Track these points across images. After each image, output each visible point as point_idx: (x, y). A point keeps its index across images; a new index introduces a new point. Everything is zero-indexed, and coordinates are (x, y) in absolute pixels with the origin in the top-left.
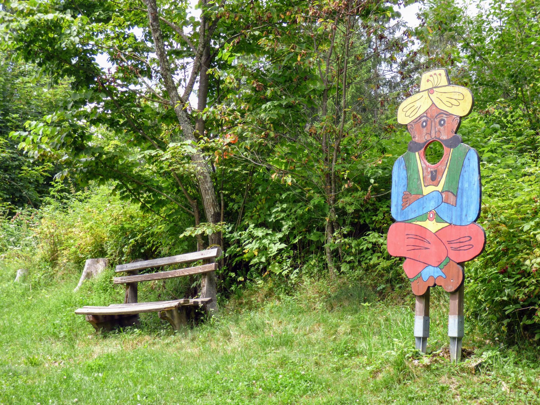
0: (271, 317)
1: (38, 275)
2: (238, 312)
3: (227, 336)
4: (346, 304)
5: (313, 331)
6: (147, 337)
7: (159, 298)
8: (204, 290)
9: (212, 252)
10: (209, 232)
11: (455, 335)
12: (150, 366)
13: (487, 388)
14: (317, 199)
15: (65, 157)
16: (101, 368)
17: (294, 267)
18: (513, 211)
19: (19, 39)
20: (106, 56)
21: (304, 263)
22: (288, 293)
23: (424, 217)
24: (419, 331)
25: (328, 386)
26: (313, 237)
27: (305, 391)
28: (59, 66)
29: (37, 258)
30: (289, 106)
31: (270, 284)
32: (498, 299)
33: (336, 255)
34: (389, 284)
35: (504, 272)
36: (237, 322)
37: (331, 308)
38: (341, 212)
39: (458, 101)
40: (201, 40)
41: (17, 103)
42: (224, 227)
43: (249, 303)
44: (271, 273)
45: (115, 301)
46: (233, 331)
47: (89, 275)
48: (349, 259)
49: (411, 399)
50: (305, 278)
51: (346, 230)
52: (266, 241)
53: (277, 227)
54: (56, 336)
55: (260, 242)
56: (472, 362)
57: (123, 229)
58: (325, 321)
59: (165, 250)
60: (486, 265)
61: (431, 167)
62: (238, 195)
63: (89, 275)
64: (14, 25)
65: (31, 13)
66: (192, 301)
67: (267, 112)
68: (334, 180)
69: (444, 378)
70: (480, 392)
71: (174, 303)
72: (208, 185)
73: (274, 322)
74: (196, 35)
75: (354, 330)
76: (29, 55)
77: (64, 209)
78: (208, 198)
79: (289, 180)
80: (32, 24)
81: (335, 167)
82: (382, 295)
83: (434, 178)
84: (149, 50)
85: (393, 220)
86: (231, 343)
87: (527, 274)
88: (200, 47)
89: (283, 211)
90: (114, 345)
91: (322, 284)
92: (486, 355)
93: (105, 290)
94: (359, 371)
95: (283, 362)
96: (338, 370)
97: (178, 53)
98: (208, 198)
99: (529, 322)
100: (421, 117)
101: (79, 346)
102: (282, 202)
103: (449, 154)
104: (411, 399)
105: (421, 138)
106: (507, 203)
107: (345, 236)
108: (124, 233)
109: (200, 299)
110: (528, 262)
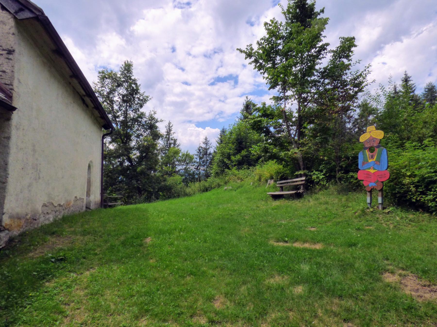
0: (322, 196)
1: (256, 184)
2: (311, 195)
3: (309, 201)
4: (344, 193)
5: (334, 200)
6: (287, 201)
7: (289, 191)
8: (302, 188)
9: (304, 178)
10: (302, 173)
11: (381, 202)
12: (289, 209)
13: (392, 219)
14: (334, 163)
15: (263, 154)
16: (275, 209)
17: (327, 182)
18: (398, 166)
19: (251, 125)
20: (272, 128)
21: (330, 181)
22: (326, 189)
23: (369, 168)
24: (368, 201)
25: (341, 216)
26: (332, 174)
27: (334, 217)
28: (261, 131)
29: (256, 180)
30: (324, 138)
31: (320, 187)
32: (394, 192)
33: (340, 179)
34: (357, 187)
35: (396, 184)
36: (311, 197)
37: (339, 194)
38: (341, 167)
39: (380, 135)
40: (298, 122)
41: (249, 140)
42: (306, 171)
43: (315, 192)
44: (320, 184)
45: (277, 191)
46: (311, 200)
47: (269, 184)
48: (344, 180)
49: (367, 221)
50: (330, 185)
51: (342, 172)
52: (319, 175)
53: (321, 171)
54: (262, 200)
55: (317, 175)
56: (386, 211)
57: (278, 172)
58: (338, 198)
59: (289, 178)
60: (389, 182)
61: (371, 154)
62: (310, 162)
63: (269, 184)
64: (250, 122)
65: (254, 119)
66: (299, 191)
67: (318, 140)
68: (339, 158)
69: (378, 215)
70: (390, 220)
71: (294, 192)
72: (301, 160)
73: (322, 198)
74: (296, 120)
75: (347, 200)
76: (253, 129)
77: (261, 167)
78: (301, 163)
79: (326, 158)
80: (254, 121)
81: (339, 154)
82: (355, 190)
83: (372, 157)
84: (284, 125)
85: (359, 170)
86: (311, 203)
87: (404, 185)
88: (298, 124)
89: (323, 167)
90: (277, 203)
91: (336, 187)
92: (391, 209)
93: (274, 188)
94: (349, 212)
95: (326, 209)
96: (343, 211)
97: (292, 126)
98: (301, 163)
99: (405, 199)
100: (367, 140)
101: (269, 203)
102: (323, 164)
103: (377, 150)
104: (367, 221)
105: (367, 146)
106: (396, 164)
107: (342, 173)
108: (278, 173)
109: (301, 191)
110: (404, 181)
